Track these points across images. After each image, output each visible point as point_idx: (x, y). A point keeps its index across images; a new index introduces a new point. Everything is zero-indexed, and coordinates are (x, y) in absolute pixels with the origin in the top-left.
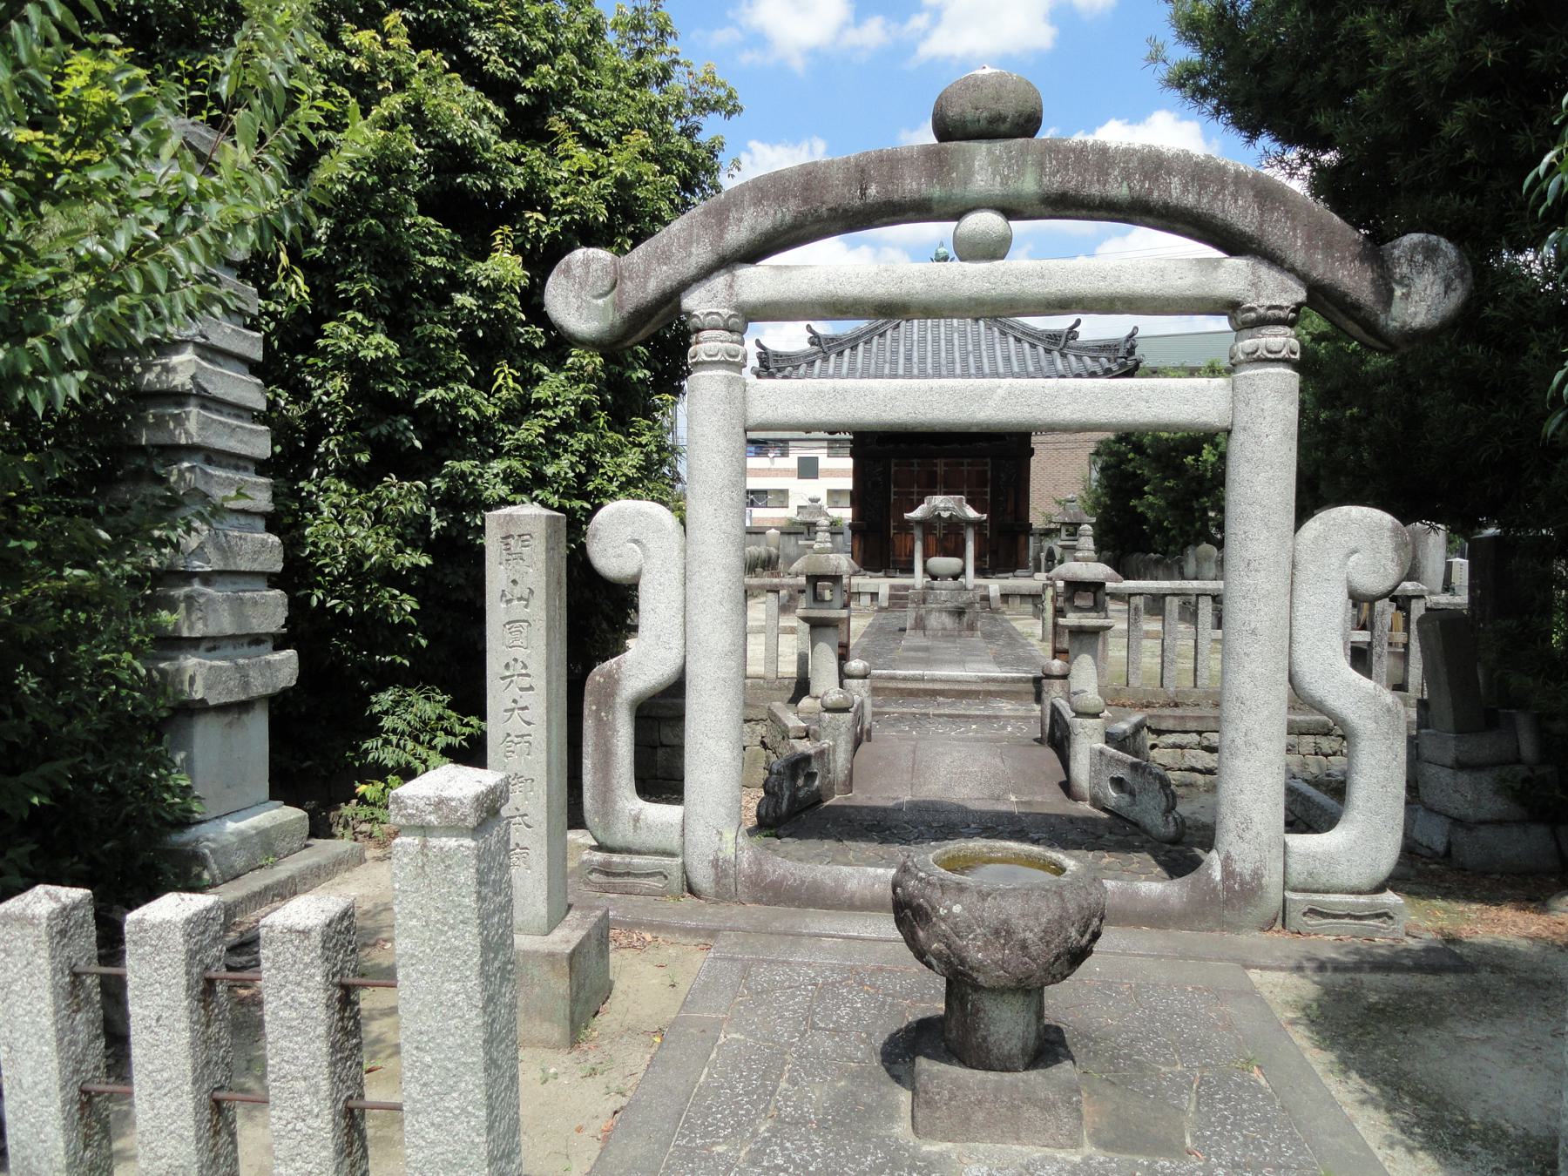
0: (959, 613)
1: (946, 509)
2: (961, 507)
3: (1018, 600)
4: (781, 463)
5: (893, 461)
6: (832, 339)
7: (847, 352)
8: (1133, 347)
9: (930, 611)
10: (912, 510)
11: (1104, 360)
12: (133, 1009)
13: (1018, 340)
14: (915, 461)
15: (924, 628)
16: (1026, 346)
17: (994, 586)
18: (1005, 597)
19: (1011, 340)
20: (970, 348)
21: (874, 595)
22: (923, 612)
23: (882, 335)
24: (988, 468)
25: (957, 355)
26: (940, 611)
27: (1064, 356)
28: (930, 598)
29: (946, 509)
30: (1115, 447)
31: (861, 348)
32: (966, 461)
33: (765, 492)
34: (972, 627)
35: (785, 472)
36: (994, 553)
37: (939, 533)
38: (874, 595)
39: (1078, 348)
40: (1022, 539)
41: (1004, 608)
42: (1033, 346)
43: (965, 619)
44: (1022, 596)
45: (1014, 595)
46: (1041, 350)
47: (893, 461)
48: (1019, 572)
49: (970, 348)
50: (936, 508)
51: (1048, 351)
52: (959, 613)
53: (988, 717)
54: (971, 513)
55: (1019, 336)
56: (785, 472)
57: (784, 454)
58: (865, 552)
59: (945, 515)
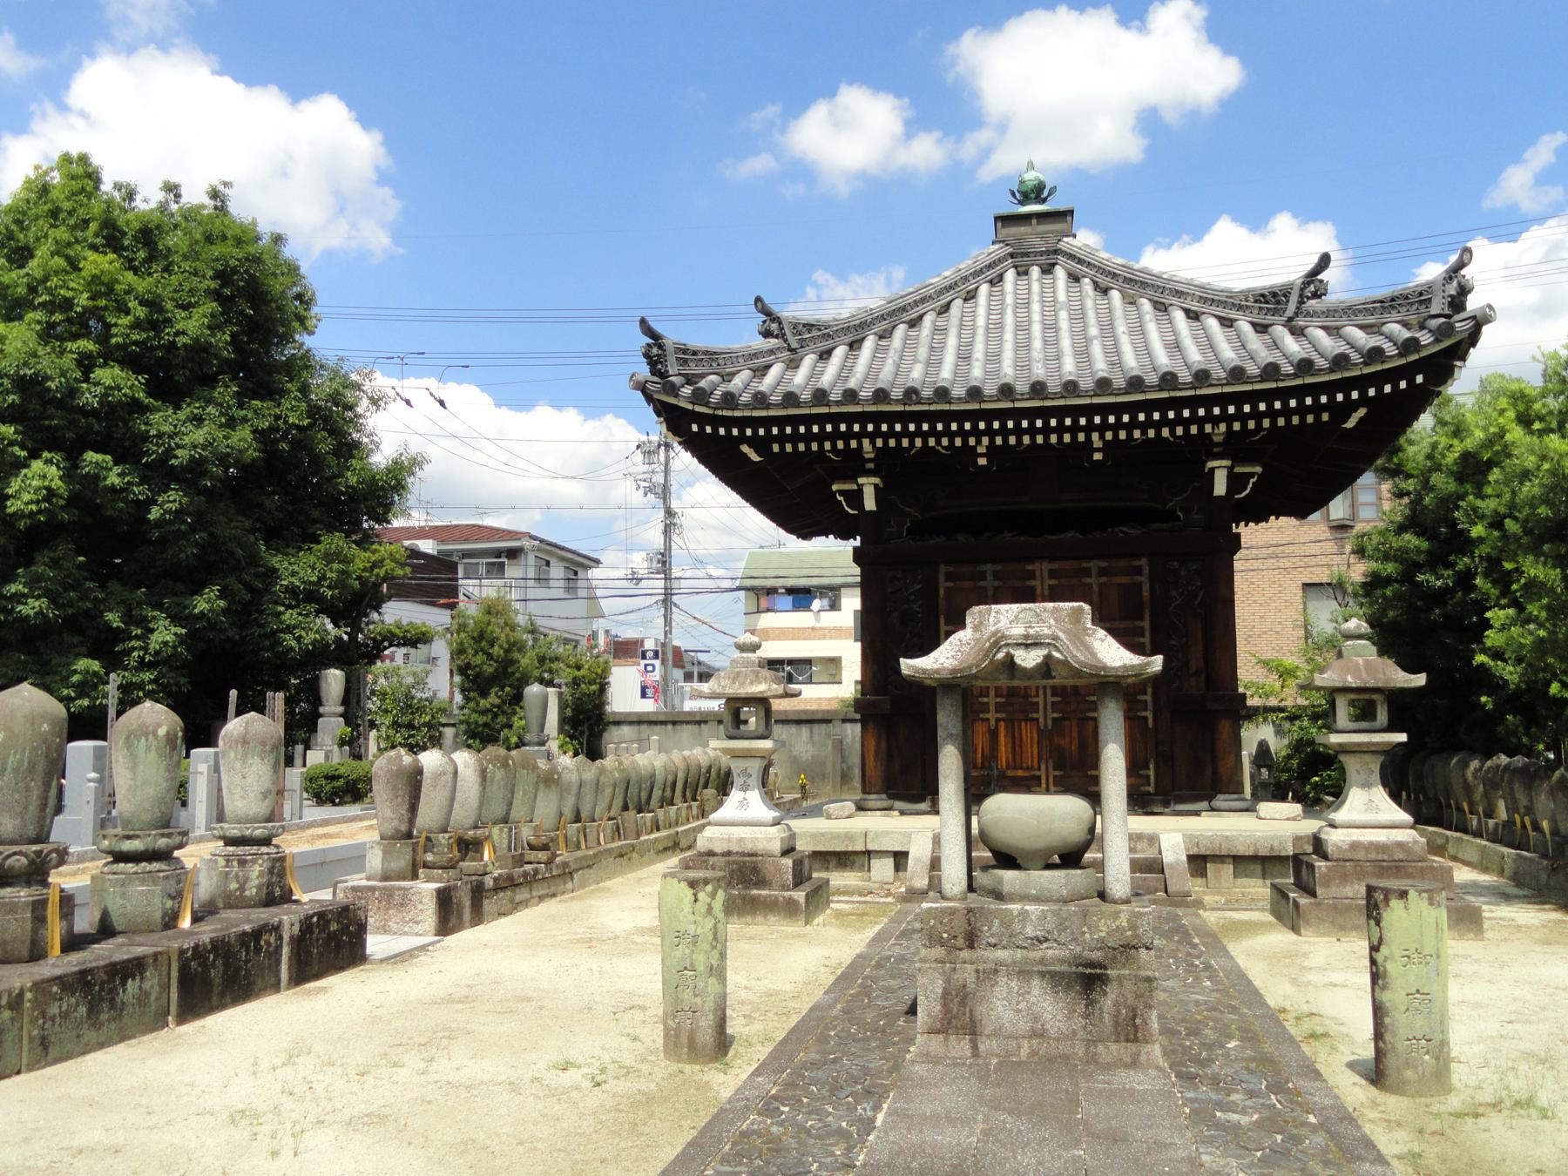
0: (1087, 980)
1: (1029, 643)
2: (1079, 637)
3: (1229, 869)
4: (830, 619)
5: (943, 569)
6: (809, 326)
7: (840, 351)
8: (1464, 291)
9: (988, 975)
10: (928, 644)
11: (1395, 328)
12: (728, 963)
13: (1192, 316)
14: (989, 568)
15: (972, 1030)
16: (1212, 323)
17: (1173, 833)
18: (1199, 862)
19: (1179, 316)
20: (1093, 331)
21: (900, 858)
22: (967, 974)
23: (914, 323)
24: (1144, 579)
25: (1066, 342)
26: (1024, 973)
27: (1298, 332)
28: (990, 930)
29: (1029, 643)
30: (1396, 542)
31: (869, 343)
32: (1095, 565)
33: (808, 662)
34: (1130, 1030)
35: (836, 633)
36: (1165, 759)
37: (1045, 716)
38: (900, 858)
39: (1330, 313)
40: (1225, 726)
41: (1195, 886)
42: (1226, 323)
43: (1108, 1001)
44: (1238, 860)
45: (1219, 858)
46: (1244, 326)
47: (943, 569)
48: (1220, 801)
49: (1093, 331)
50: (998, 641)
51: (1262, 329)
52: (1087, 980)
53: (1080, 261)
54: (1112, 654)
55: (1195, 306)
56: (836, 633)
57: (834, 606)
58: (890, 757)
59: (1029, 659)
